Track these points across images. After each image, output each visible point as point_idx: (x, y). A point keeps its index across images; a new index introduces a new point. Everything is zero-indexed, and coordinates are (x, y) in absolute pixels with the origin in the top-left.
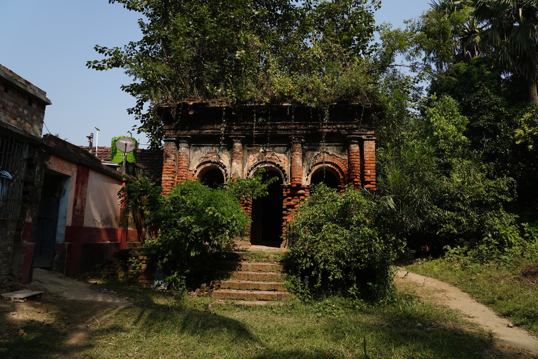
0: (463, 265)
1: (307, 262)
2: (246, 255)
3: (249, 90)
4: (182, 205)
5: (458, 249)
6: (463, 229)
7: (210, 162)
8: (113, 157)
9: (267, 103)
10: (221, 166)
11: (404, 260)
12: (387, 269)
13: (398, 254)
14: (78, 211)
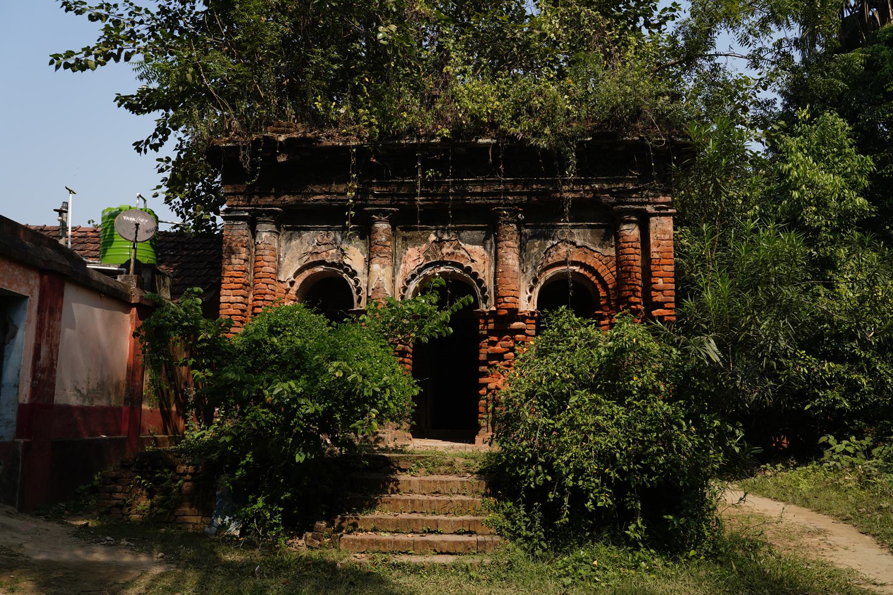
0: (864, 477)
1: (537, 474)
2: (405, 460)
3: (404, 110)
4: (272, 357)
5: (852, 443)
6: (861, 400)
7: (322, 262)
8: (105, 251)
9: (443, 139)
10: (346, 271)
11: (737, 469)
12: (703, 487)
13: (725, 456)
14: (43, 372)
